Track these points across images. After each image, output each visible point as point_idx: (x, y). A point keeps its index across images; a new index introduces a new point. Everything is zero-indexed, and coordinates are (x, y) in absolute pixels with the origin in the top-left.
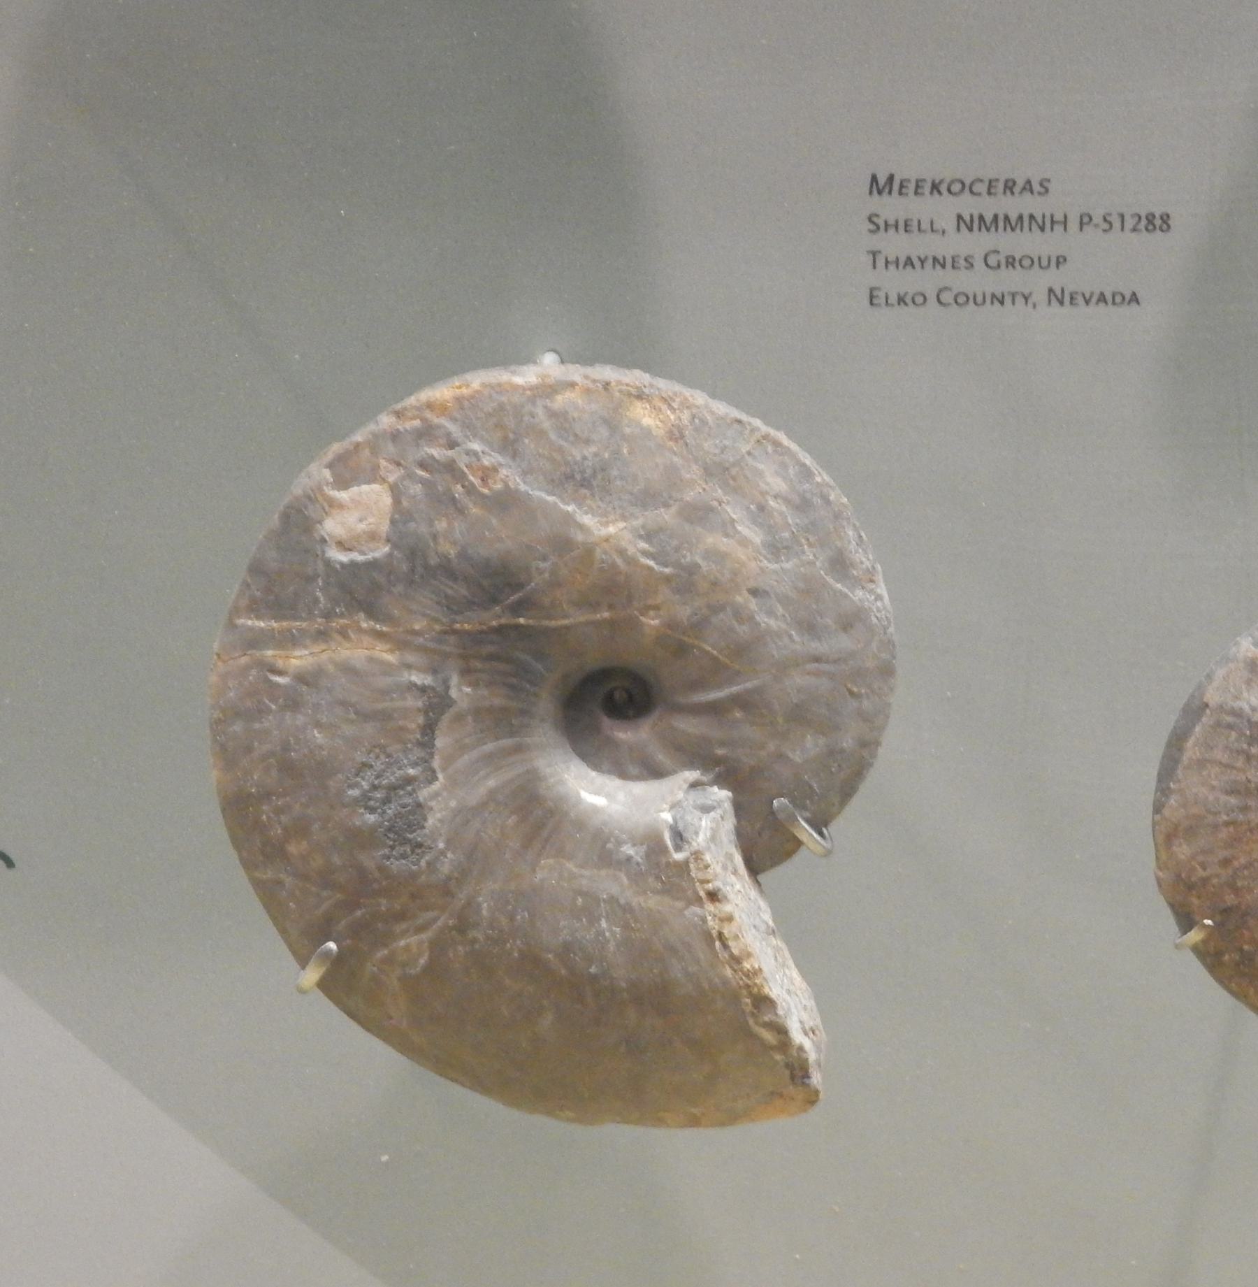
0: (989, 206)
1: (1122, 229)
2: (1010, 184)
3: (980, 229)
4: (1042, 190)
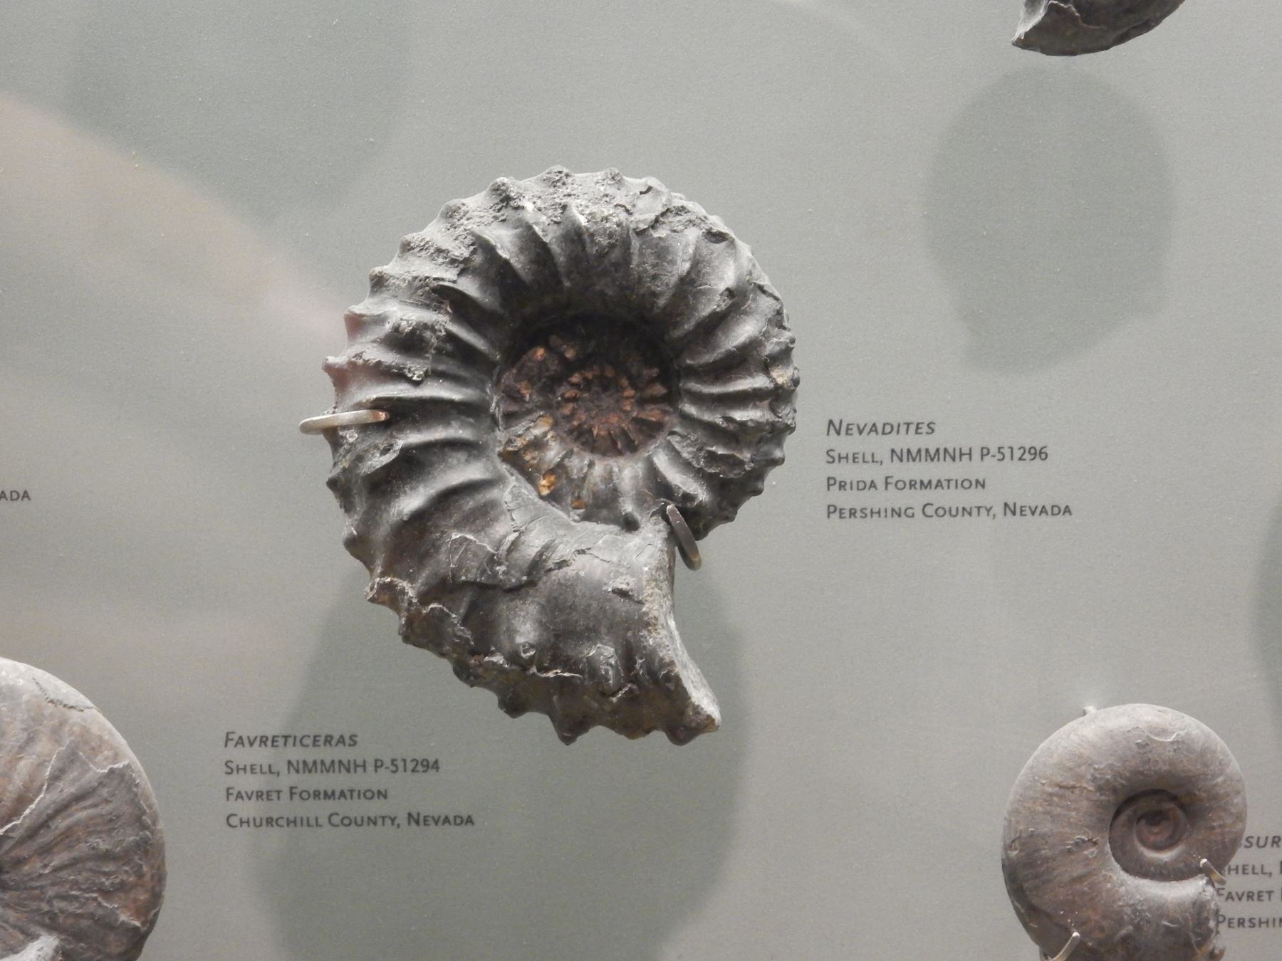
0: (311, 755)
1: (1012, 459)
4: (352, 743)
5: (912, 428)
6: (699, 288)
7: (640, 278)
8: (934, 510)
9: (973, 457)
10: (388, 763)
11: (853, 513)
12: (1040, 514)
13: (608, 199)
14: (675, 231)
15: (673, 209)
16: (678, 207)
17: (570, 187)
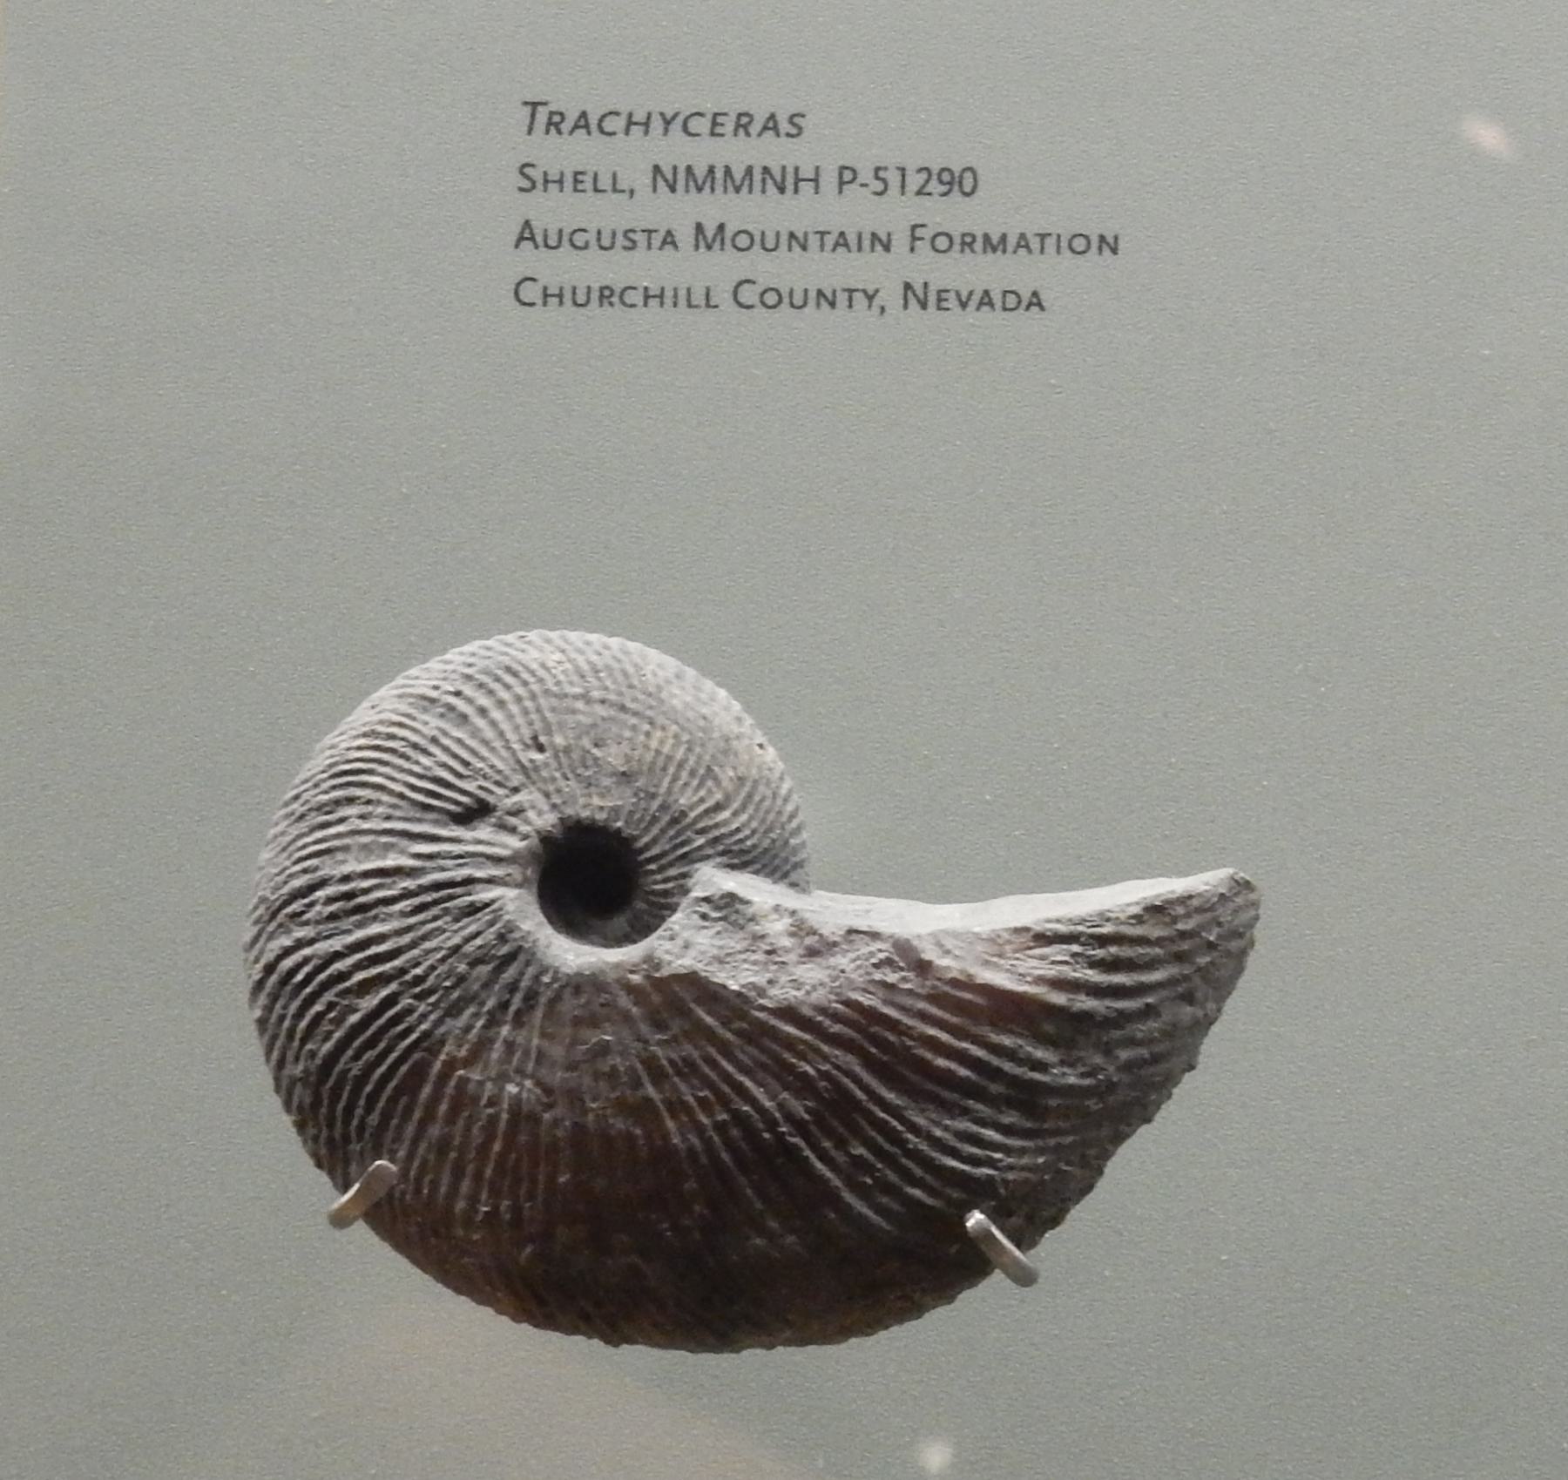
0: (702, 153)
2: (744, 120)
3: (687, 191)
10: (866, 175)
12: (978, 309)
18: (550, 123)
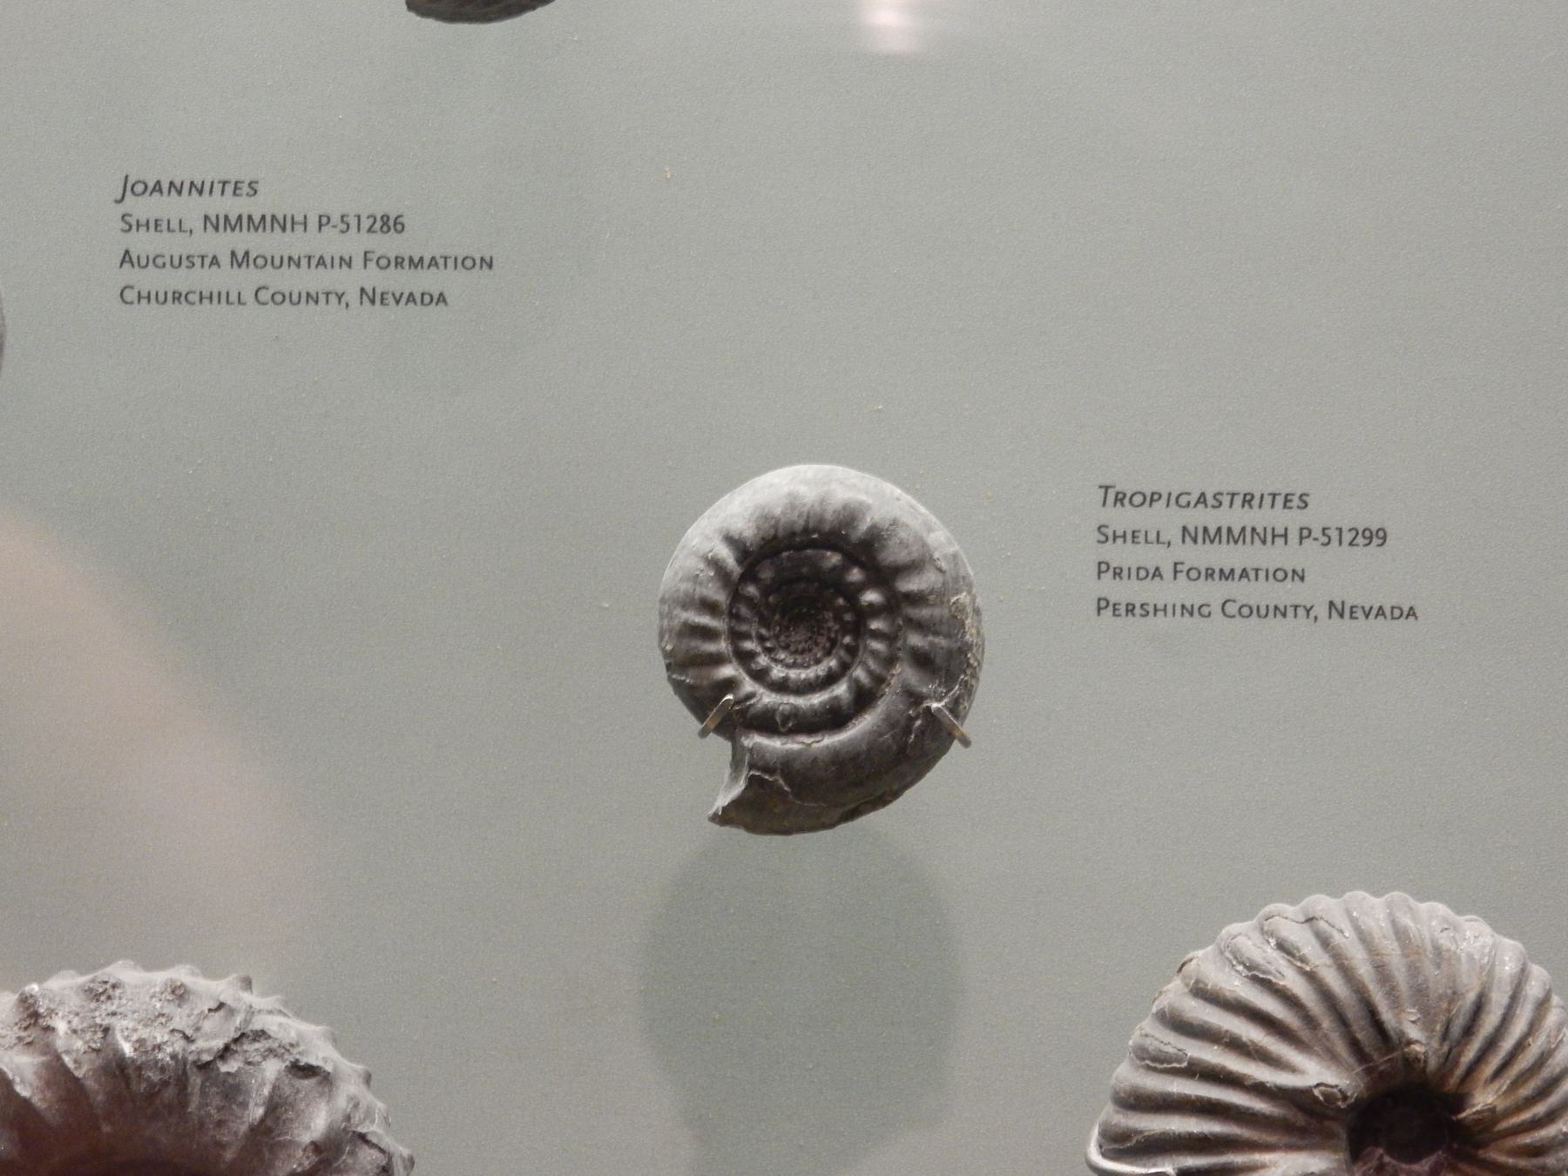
1: (1340, 543)
5: (1280, 501)
6: (277, 1139)
7: (202, 1125)
8: (1238, 607)
9: (1289, 540)
11: (1130, 609)
13: (163, 1020)
14: (250, 1063)
15: (251, 1034)
16: (257, 1031)
17: (116, 1002)
18: (1116, 500)
